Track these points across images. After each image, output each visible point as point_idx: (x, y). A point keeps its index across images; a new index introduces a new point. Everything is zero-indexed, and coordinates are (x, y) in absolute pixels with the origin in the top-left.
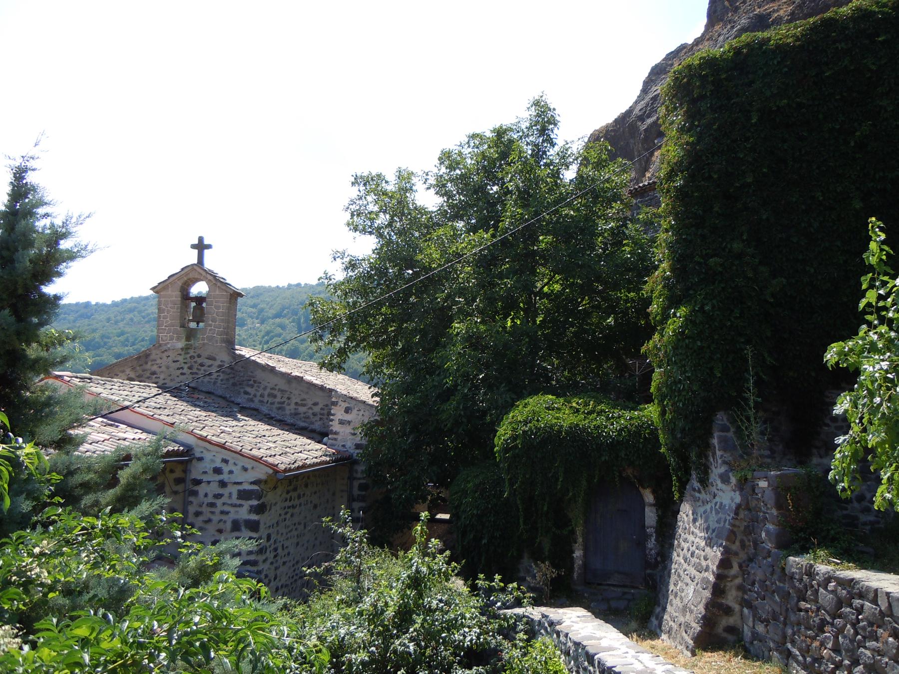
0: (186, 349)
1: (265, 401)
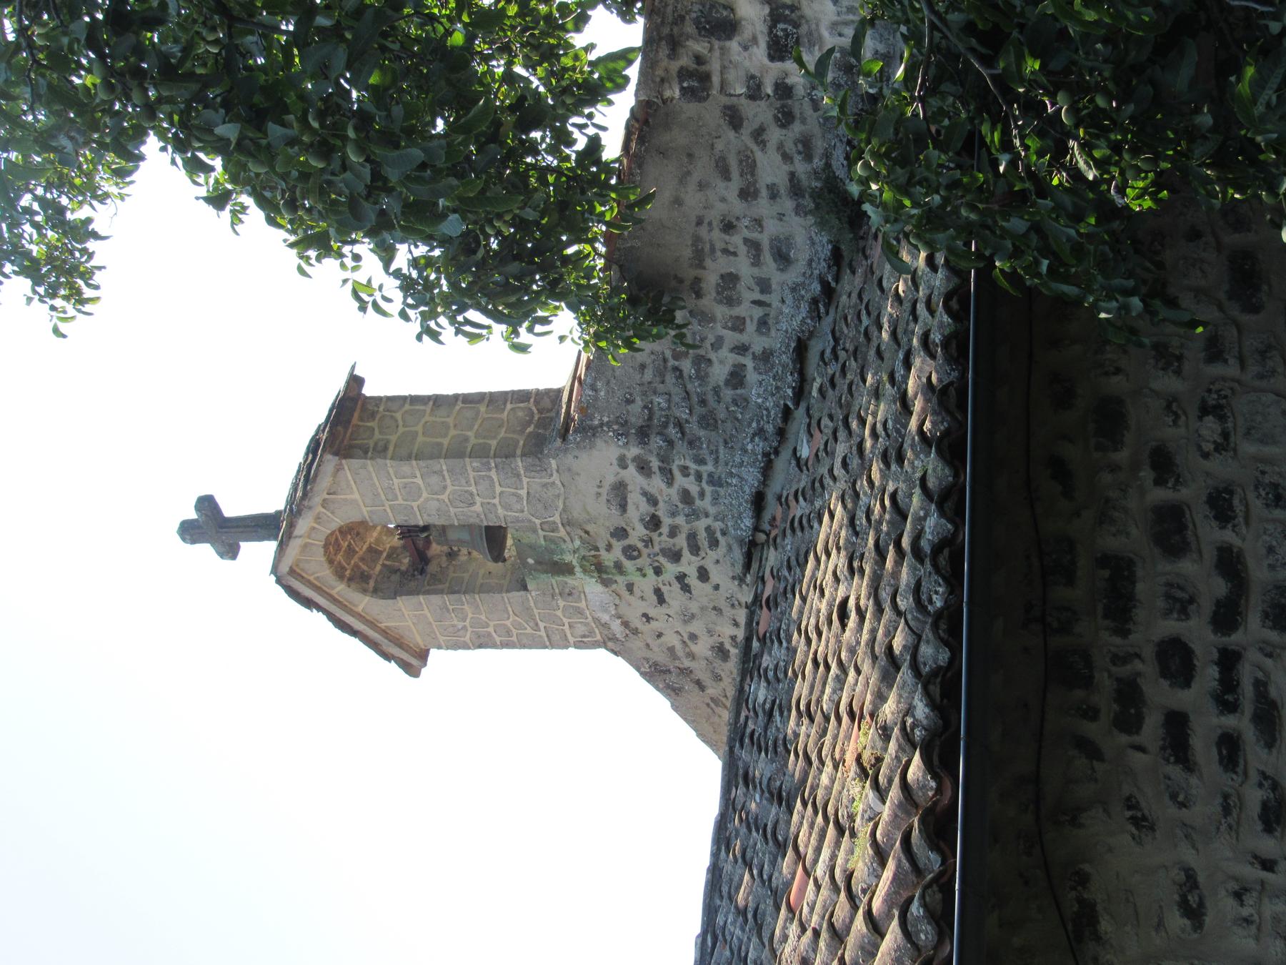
1: (758, 312)
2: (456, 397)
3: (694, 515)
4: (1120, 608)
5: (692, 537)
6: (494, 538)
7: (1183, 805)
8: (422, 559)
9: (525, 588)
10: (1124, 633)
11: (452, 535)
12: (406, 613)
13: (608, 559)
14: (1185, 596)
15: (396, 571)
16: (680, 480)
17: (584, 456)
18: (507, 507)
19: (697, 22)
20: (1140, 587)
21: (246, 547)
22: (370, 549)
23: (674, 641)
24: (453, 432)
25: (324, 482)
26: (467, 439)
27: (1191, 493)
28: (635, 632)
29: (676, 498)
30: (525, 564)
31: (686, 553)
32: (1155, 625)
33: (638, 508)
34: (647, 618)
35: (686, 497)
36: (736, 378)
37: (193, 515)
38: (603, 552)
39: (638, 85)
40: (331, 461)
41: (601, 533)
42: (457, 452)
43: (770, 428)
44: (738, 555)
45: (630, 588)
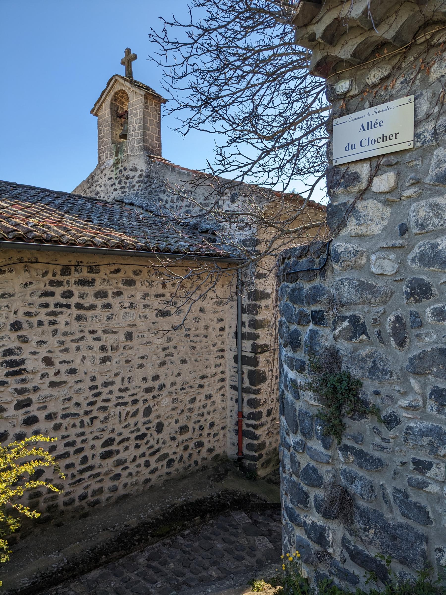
2: (160, 128)
3: (129, 188)
4: (81, 282)
5: (124, 187)
6: (124, 136)
7: (31, 295)
8: (120, 117)
9: (112, 144)
10: (75, 283)
11: (126, 125)
12: (106, 111)
13: (119, 166)
14: (84, 297)
15: (117, 109)
16: (137, 185)
17: (143, 161)
18: (132, 140)
19: (234, 193)
20: (87, 287)
21: (124, 67)
22: (123, 102)
23: (99, 182)
24: (151, 127)
25: (138, 91)
26: (149, 131)
27: (110, 299)
28: (102, 172)
29: (133, 184)
30: (118, 144)
31: (121, 186)
32: (77, 290)
33: (131, 174)
34: (105, 175)
36: (160, 200)
37: (132, 52)
38: (121, 164)
40: (143, 93)
41: (125, 164)
42: (145, 128)
43: (148, 208)
44: (120, 199)
45: (112, 171)
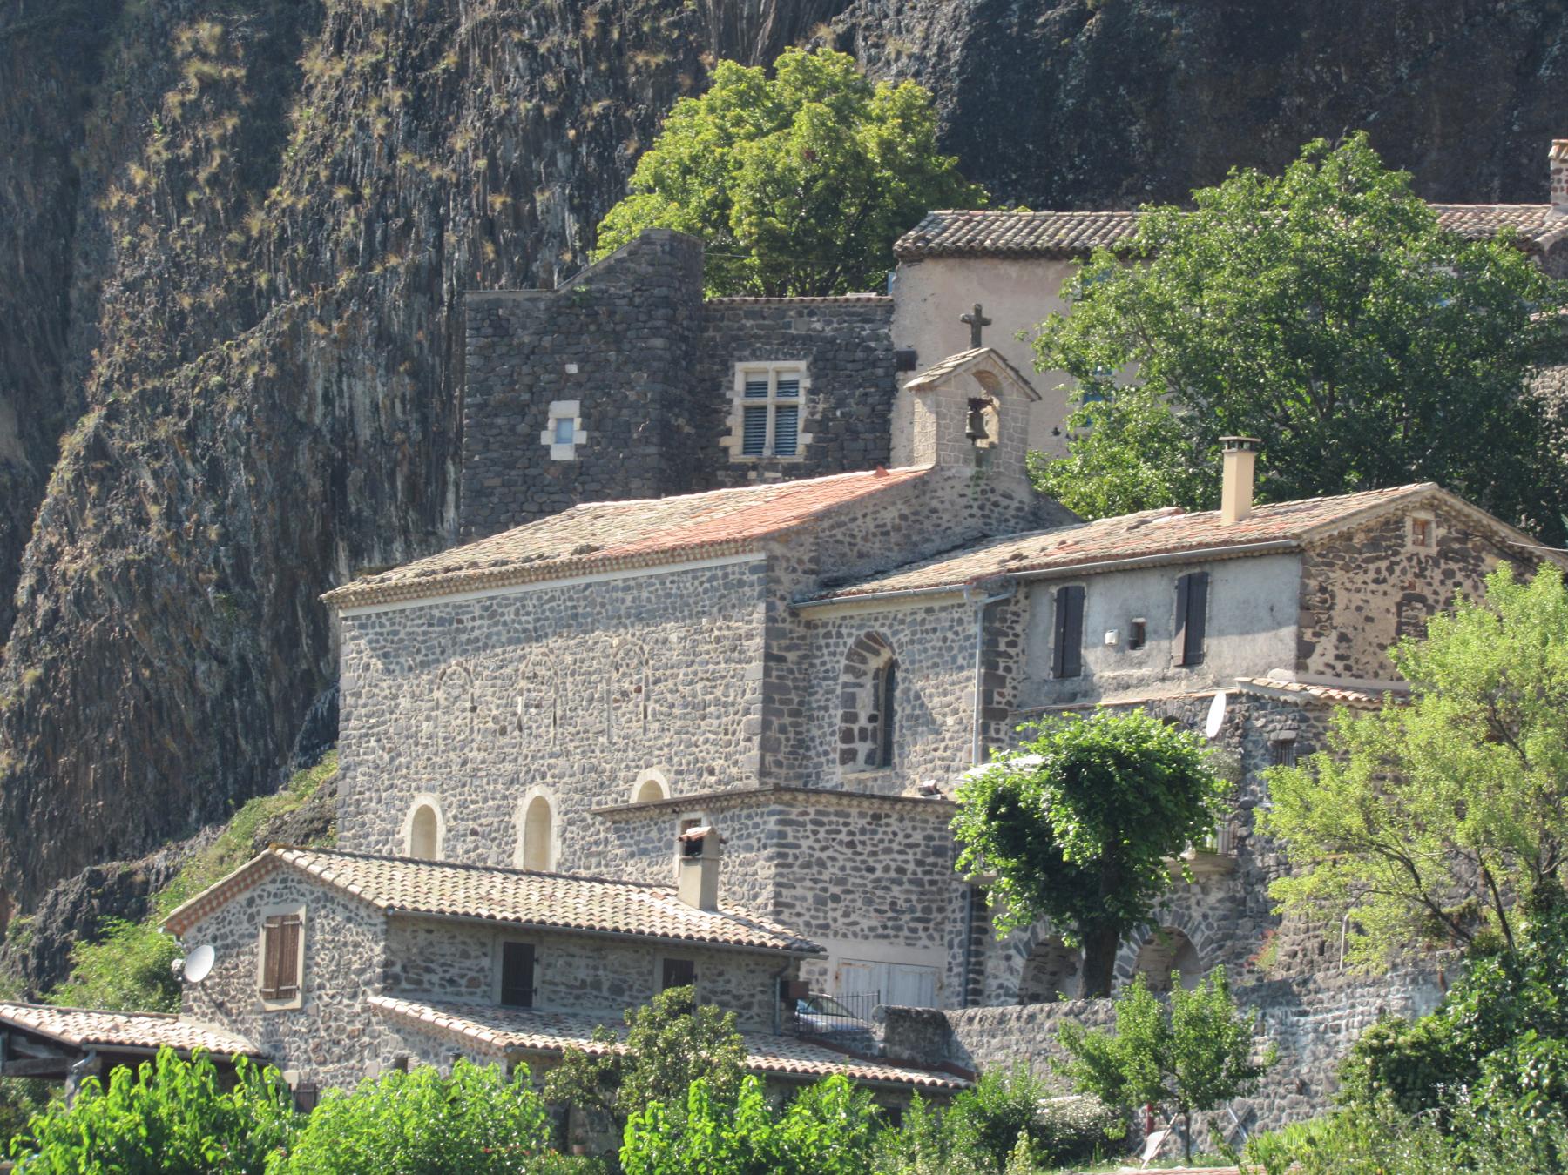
0: (977, 478)
13: (982, 482)
23: (940, 493)
35: (1007, 520)
39: (528, 813)
